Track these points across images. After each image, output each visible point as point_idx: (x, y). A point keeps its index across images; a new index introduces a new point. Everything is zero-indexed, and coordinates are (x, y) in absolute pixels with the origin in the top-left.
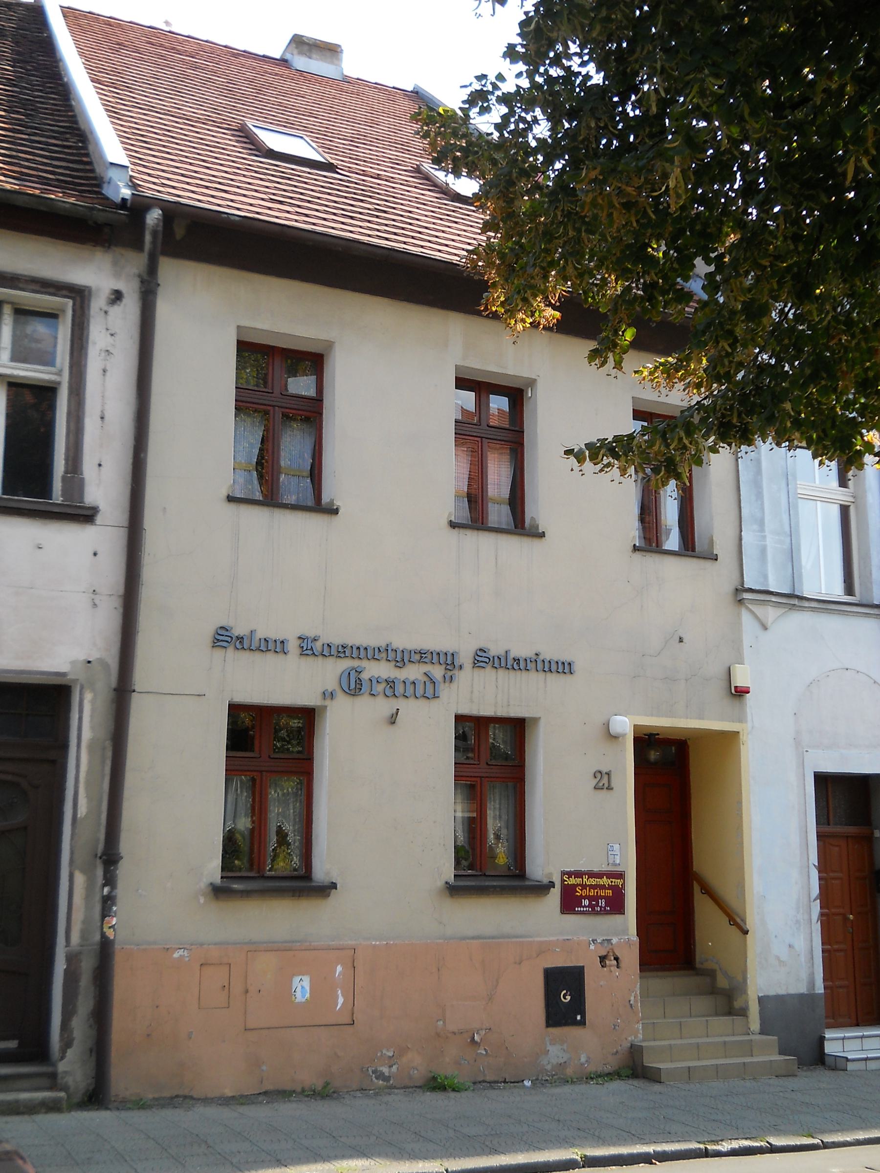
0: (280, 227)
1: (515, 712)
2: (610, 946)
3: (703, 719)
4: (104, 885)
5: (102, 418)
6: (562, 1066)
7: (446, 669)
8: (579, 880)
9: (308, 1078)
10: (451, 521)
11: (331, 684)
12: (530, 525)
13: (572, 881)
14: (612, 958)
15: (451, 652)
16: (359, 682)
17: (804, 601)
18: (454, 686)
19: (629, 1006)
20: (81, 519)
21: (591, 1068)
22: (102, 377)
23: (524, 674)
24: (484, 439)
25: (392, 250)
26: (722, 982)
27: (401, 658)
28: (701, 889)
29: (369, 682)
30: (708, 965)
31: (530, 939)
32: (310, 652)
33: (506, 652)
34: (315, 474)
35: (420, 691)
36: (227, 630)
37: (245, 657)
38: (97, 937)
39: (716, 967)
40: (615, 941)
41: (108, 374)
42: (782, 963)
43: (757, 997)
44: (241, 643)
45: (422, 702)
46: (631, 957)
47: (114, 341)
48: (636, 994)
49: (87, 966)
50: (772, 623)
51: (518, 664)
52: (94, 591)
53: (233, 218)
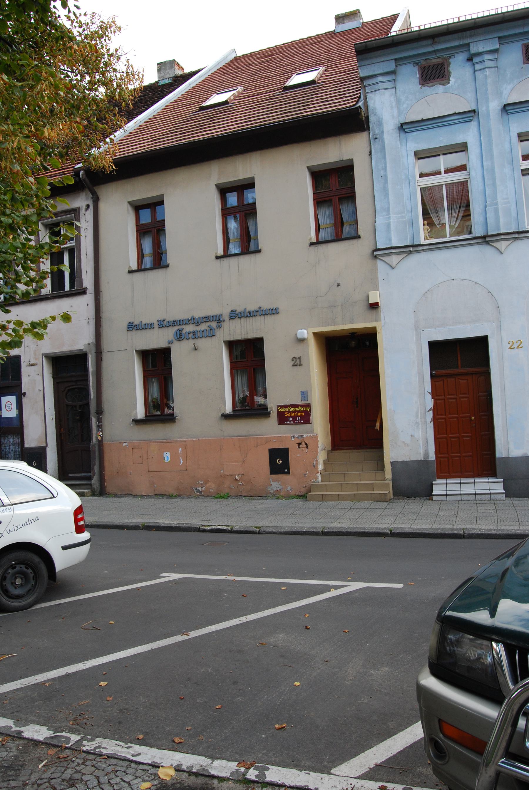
2: (302, 439)
3: (353, 323)
8: (286, 409)
13: (283, 410)
16: (181, 335)
21: (293, 493)
25: (167, 148)
27: (197, 322)
40: (305, 436)
42: (407, 445)
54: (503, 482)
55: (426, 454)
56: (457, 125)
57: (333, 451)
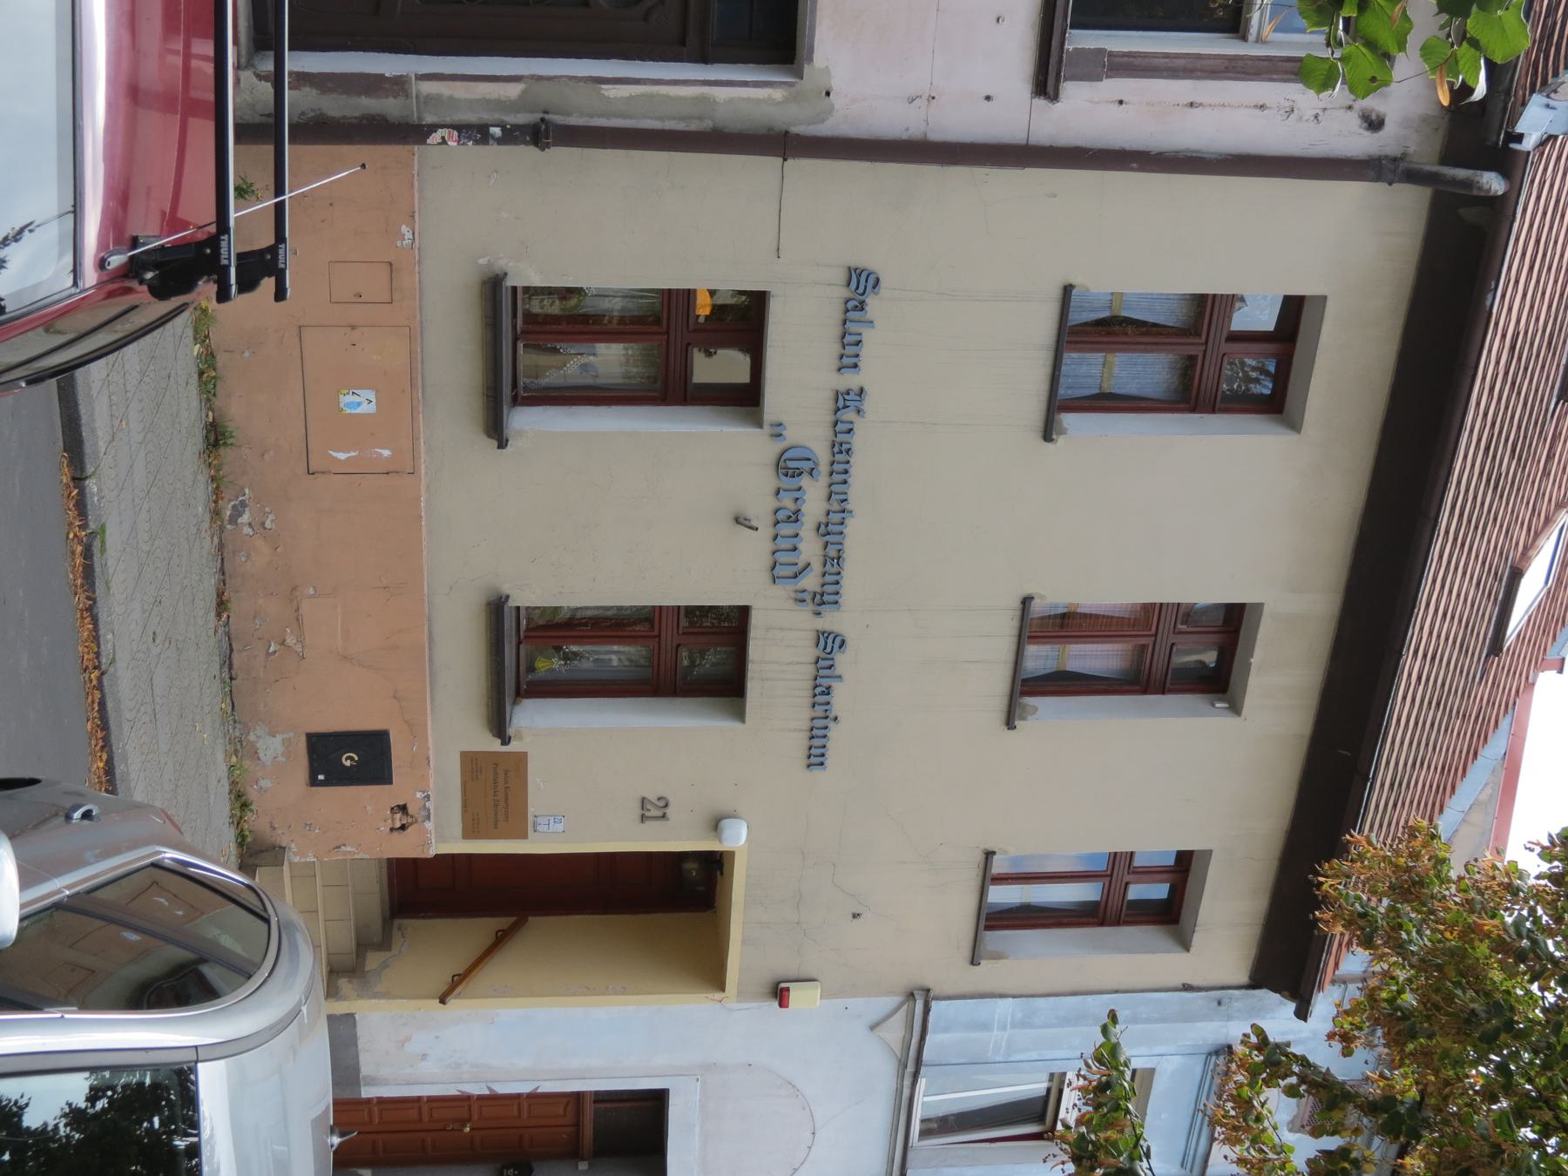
0: (1473, 365)
1: (753, 687)
4: (502, 126)
5: (1191, 104)
6: (255, 755)
7: (815, 594)
9: (236, 410)
10: (1033, 598)
11: (792, 435)
12: (1026, 705)
14: (404, 822)
15: (845, 531)
16: (797, 473)
17: (911, 1079)
18: (790, 604)
20: (1040, 77)
22: (1254, 104)
23: (808, 701)
24: (1109, 878)
26: (373, 960)
27: (831, 531)
28: (503, 930)
29: (796, 487)
30: (396, 935)
31: (429, 711)
32: (841, 403)
33: (872, 322)
34: (1106, 402)
35: (782, 558)
36: (874, 288)
37: (835, 314)
38: (429, 119)
39: (394, 951)
40: (429, 825)
41: (1258, 112)
43: (353, 1012)
44: (854, 307)
45: (767, 561)
46: (406, 847)
47: (1307, 120)
49: (389, 107)
50: (879, 1036)
51: (823, 693)
52: (933, 98)
53: (1490, 297)
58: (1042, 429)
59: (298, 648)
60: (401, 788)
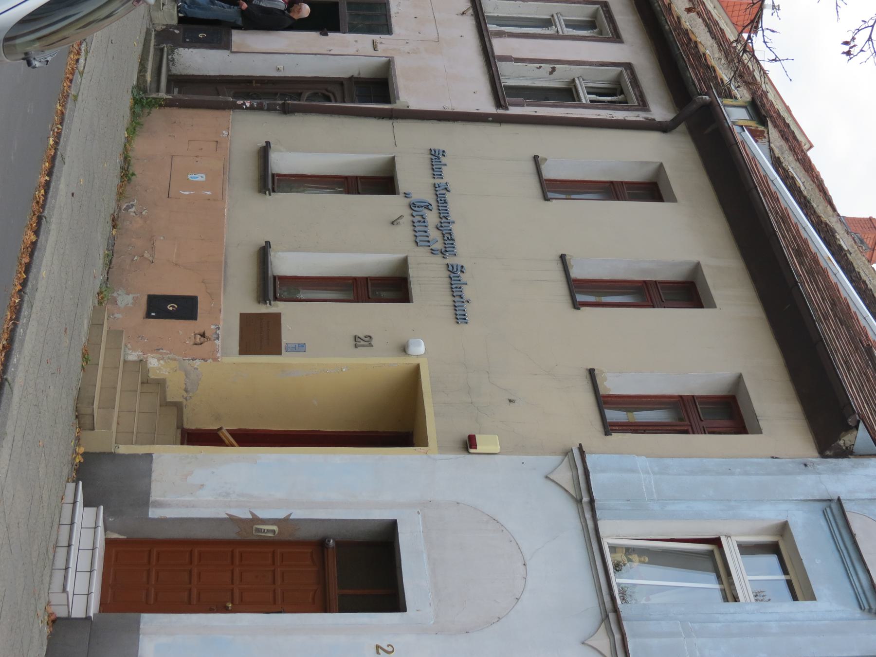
2: (212, 339)
11: (416, 197)
17: (590, 513)
19: (158, 348)
40: (217, 342)
48: (168, 354)
54: (88, 618)
55: (159, 505)
56: (849, 587)
57: (179, 431)
58: (563, 269)
59: (151, 259)
60: (202, 323)
